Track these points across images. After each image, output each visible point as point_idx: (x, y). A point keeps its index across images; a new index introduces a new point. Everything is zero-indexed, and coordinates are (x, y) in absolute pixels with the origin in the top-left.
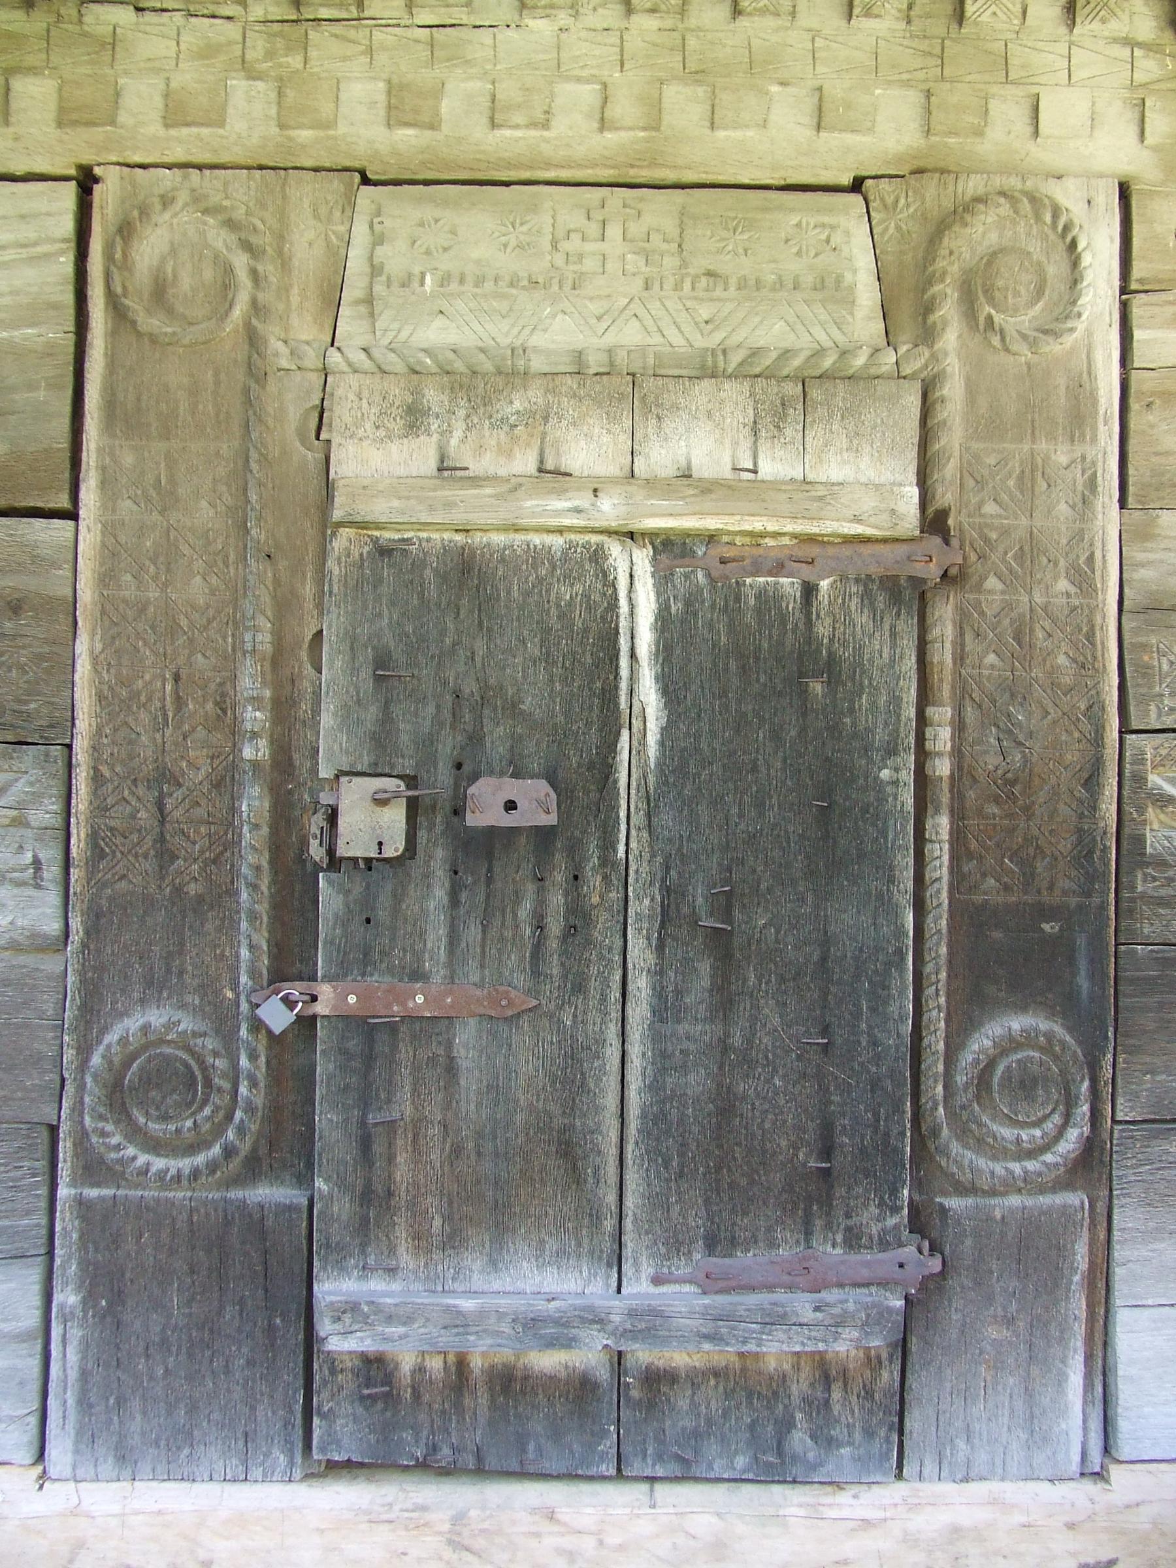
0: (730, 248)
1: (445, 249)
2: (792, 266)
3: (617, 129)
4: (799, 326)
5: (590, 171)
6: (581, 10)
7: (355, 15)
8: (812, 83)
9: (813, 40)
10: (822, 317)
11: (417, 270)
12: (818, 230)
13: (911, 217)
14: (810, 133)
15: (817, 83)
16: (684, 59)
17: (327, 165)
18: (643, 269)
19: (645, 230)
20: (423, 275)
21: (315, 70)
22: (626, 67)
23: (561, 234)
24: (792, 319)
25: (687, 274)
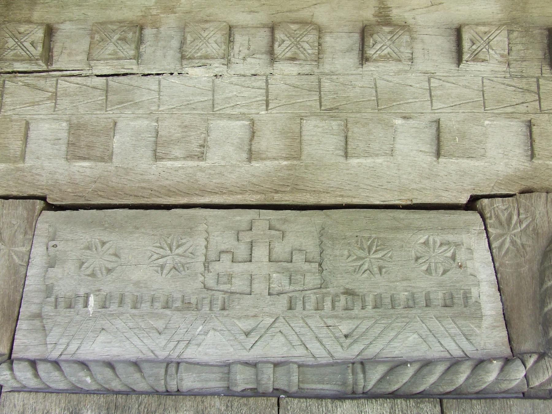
0: (366, 267)
1: (109, 271)
2: (423, 284)
3: (262, 159)
4: (431, 339)
5: (239, 197)
6: (233, 60)
7: (45, 68)
8: (429, 117)
9: (429, 81)
10: (452, 331)
11: (82, 292)
12: (444, 248)
13: (524, 231)
14: (431, 158)
15: (435, 117)
16: (320, 98)
17: (15, 193)
18: (287, 288)
19: (288, 249)
20: (87, 296)
21: (9, 113)
22: (271, 106)
23: (212, 255)
24: (424, 331)
25: (328, 293)
